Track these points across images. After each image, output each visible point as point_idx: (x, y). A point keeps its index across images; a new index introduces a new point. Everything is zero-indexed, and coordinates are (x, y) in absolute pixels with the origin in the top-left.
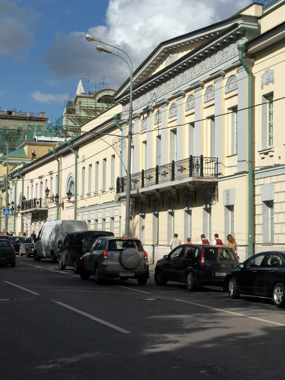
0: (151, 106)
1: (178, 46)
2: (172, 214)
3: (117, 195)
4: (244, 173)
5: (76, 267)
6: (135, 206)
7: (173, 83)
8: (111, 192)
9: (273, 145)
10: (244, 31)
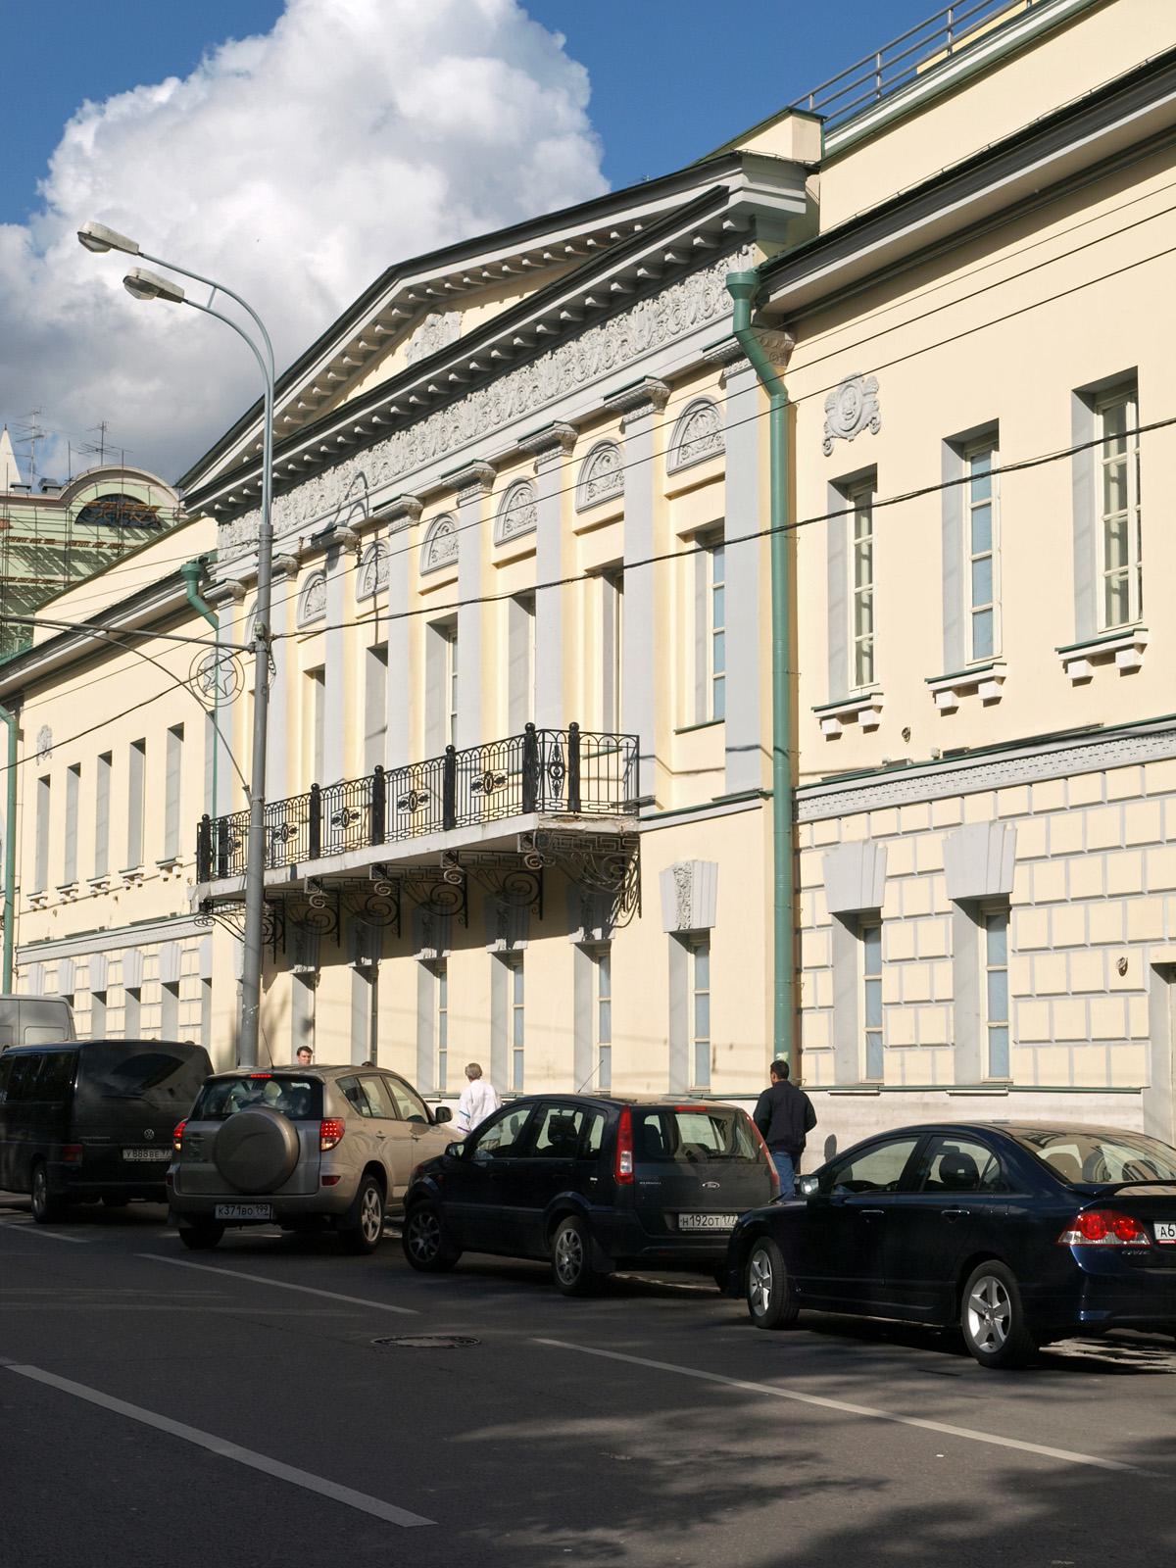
0: (344, 525)
1: (466, 280)
2: (437, 970)
3: (197, 891)
4: (756, 797)
5: (44, 1195)
6: (274, 934)
7: (443, 430)
8: (166, 880)
9: (875, 682)
10: (752, 220)
